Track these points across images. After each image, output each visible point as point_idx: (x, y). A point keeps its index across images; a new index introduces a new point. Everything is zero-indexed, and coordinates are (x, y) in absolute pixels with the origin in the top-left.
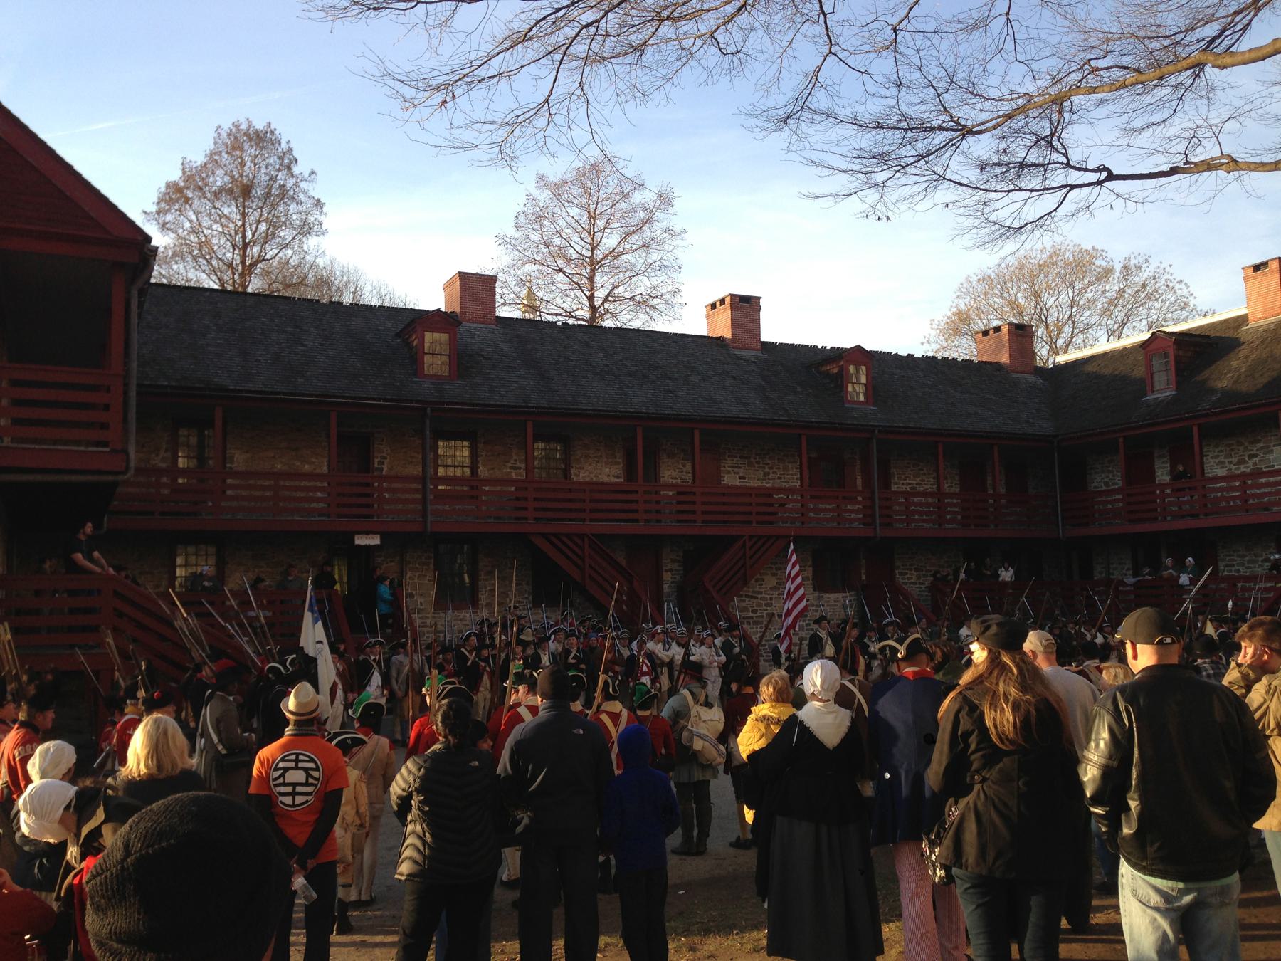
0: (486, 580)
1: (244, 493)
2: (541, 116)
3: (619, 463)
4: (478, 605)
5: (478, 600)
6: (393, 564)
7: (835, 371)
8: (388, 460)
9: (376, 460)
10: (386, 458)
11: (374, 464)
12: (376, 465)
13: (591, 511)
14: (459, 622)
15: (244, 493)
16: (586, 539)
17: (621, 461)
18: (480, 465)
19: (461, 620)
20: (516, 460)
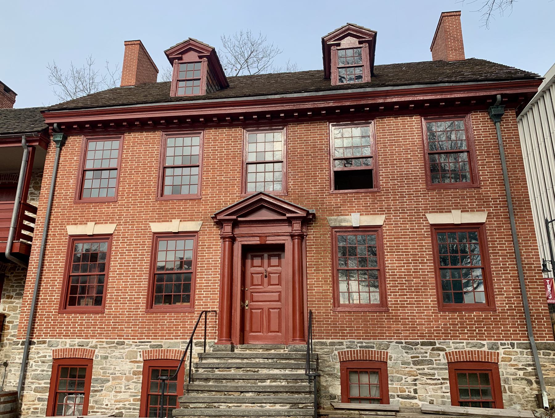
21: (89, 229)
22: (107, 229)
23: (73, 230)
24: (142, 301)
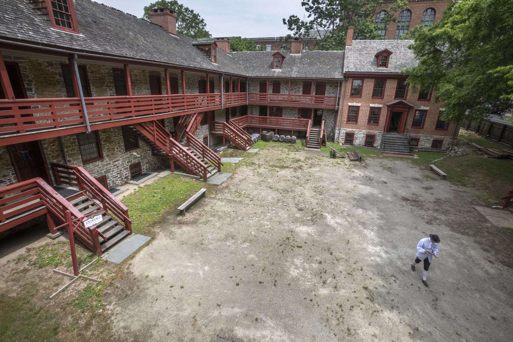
0: (105, 144)
1: (210, 153)
2: (352, 182)
3: (148, 83)
4: (103, 157)
5: (103, 155)
6: (55, 146)
7: (207, 49)
8: (34, 83)
9: (25, 83)
10: (32, 81)
11: (24, 85)
12: (26, 86)
13: (155, 109)
14: (97, 167)
15: (210, 153)
16: (154, 122)
17: (149, 82)
18: (91, 85)
19: (97, 166)
20: (108, 82)
21: (355, 104)
22: (359, 105)
23: (350, 104)
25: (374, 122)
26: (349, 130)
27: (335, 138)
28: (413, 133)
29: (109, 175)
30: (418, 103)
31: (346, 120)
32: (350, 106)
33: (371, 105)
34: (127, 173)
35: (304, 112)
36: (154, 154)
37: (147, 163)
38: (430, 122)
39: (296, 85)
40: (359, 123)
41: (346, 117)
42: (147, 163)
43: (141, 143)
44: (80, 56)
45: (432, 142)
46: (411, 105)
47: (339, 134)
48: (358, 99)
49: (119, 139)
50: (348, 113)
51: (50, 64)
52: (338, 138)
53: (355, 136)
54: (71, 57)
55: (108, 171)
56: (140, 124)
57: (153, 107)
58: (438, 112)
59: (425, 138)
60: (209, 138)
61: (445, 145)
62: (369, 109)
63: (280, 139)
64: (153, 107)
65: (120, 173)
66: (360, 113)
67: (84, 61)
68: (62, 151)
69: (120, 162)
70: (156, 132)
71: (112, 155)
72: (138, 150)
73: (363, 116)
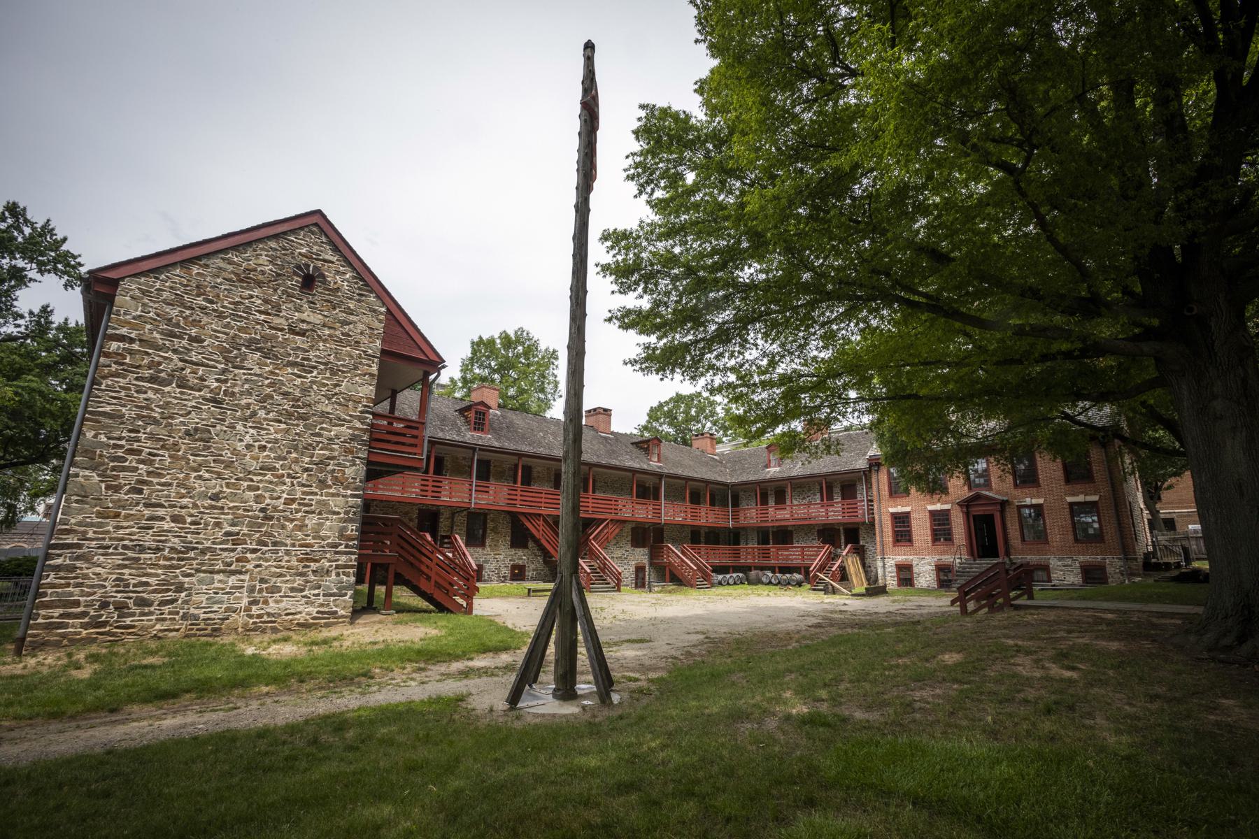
21: (900, 509)
22: (908, 509)
23: (892, 510)
24: (929, 539)
25: (945, 539)
26: (901, 558)
27: (880, 577)
28: (1030, 554)
29: (487, 566)
30: (1018, 492)
31: (891, 539)
32: (893, 514)
33: (930, 507)
34: (505, 572)
35: (828, 534)
36: (545, 562)
37: (534, 570)
38: (1057, 527)
39: (809, 490)
40: (916, 544)
41: (890, 534)
42: (534, 570)
43: (531, 544)
44: (480, 449)
45: (1079, 571)
46: (1005, 498)
47: (884, 567)
48: (904, 500)
49: (506, 530)
50: (893, 527)
51: (464, 458)
52: (884, 575)
53: (915, 570)
54: (474, 449)
55: (486, 562)
56: (523, 514)
57: (543, 500)
58: (1066, 506)
59: (1059, 563)
60: (647, 570)
61: (1116, 576)
62: (927, 514)
63: (773, 580)
64: (543, 500)
65: (498, 569)
66: (914, 524)
67: (487, 456)
68: (452, 528)
69: (502, 557)
70: (542, 528)
71: (495, 547)
72: (526, 551)
73: (921, 529)
